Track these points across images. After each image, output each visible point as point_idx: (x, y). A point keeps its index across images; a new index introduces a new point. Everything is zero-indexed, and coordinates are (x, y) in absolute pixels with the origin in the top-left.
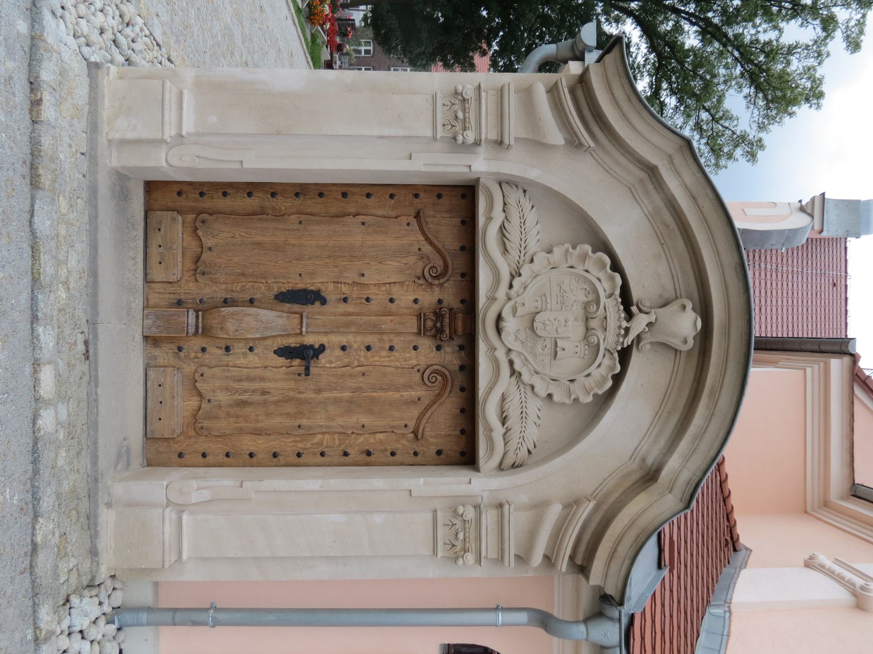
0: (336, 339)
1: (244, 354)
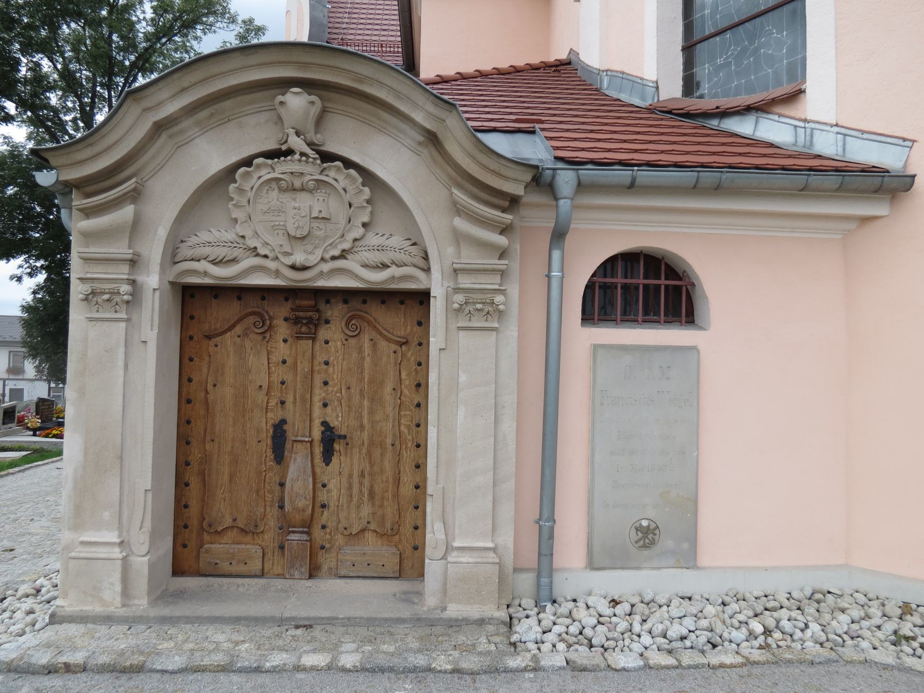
0: (317, 411)
1: (328, 492)
